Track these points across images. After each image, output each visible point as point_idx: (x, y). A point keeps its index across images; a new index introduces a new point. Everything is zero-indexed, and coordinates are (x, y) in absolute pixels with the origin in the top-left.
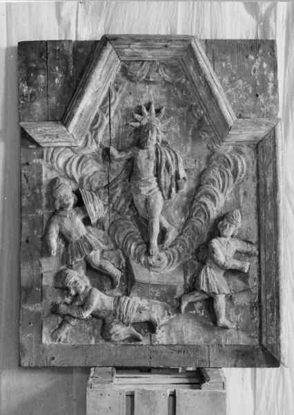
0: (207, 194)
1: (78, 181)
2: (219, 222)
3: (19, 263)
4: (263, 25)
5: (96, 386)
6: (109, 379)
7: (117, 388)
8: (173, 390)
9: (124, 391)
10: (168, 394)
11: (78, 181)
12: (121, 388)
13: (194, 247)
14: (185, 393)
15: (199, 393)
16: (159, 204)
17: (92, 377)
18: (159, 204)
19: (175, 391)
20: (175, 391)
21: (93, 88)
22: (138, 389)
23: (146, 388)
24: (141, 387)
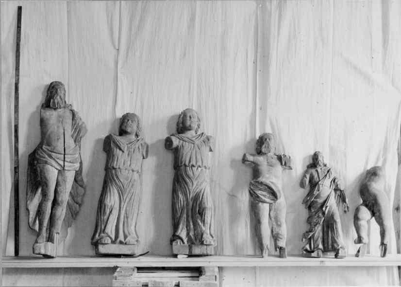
0: (242, 192)
1: (40, 190)
2: (33, 162)
3: (7, 237)
4: (262, 7)
5: (120, 278)
6: (130, 273)
7: (136, 280)
8: (178, 282)
9: (140, 282)
10: (174, 285)
11: (40, 190)
12: (139, 280)
13: (58, 97)
14: (187, 284)
15: (198, 284)
16: (61, 220)
17: (118, 272)
18: (32, 218)
19: (179, 283)
20: (179, 283)
21: (184, 218)
22: (152, 281)
23: (158, 280)
24: (153, 279)
